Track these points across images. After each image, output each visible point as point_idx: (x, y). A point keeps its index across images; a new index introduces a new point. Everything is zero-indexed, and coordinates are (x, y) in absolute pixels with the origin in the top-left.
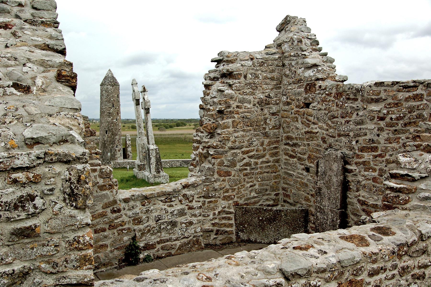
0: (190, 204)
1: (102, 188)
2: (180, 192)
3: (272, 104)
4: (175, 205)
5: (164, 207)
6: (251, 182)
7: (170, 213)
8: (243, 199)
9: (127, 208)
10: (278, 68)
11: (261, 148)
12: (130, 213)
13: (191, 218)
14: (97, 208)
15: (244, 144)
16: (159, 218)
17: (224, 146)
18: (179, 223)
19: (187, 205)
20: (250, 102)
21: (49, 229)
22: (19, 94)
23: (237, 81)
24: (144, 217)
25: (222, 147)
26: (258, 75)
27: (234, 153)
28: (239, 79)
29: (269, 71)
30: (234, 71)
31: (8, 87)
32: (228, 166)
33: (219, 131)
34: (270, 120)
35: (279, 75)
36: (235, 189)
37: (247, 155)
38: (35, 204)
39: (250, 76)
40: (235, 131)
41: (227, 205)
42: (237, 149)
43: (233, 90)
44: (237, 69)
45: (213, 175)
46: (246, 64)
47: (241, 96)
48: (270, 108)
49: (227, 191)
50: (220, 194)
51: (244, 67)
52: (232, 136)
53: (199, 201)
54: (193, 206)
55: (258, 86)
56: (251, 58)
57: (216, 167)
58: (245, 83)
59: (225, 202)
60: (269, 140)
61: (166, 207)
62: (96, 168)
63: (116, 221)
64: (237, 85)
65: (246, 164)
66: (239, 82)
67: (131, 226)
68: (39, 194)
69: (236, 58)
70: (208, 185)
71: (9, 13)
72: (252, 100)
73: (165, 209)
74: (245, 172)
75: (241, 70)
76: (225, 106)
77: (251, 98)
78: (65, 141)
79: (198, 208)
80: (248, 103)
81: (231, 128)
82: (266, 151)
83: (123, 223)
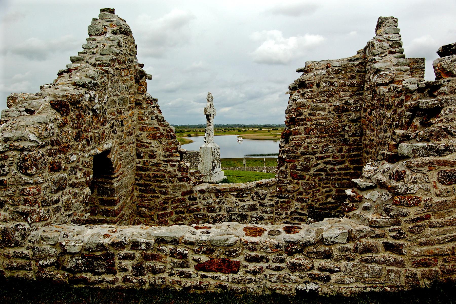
0: (261, 201)
1: (181, 179)
2: (252, 190)
3: (351, 110)
4: (247, 200)
5: (235, 201)
6: (327, 187)
7: (242, 207)
8: (319, 203)
9: (202, 198)
10: (359, 74)
11: (338, 154)
12: (205, 202)
13: (262, 214)
14: (177, 195)
15: (318, 150)
16: (230, 209)
17: (296, 151)
18: (249, 217)
19: (258, 202)
20: (324, 110)
21: (10, 182)
22: (27, 115)
23: (308, 90)
24: (217, 207)
25: (294, 152)
26: (334, 83)
27: (307, 158)
28: (311, 88)
29: (347, 78)
30: (306, 81)
31: (23, 111)
32: (300, 170)
33: (291, 137)
34: (350, 127)
35: (361, 81)
36: (309, 193)
37: (322, 160)
38: (4, 170)
39: (324, 84)
40: (308, 138)
41: (300, 207)
42: (310, 154)
43: (305, 98)
44: (309, 78)
45: (286, 177)
46: (319, 73)
47: (314, 104)
48: (349, 115)
49: (301, 194)
50: (293, 196)
51: (317, 77)
52: (304, 142)
53: (272, 200)
54: (265, 204)
55: (334, 93)
56: (327, 67)
57: (289, 170)
58: (318, 92)
59: (298, 204)
60: (348, 147)
61: (237, 201)
62: (175, 163)
63: (192, 207)
64: (308, 93)
65: (321, 170)
66: (311, 91)
67: (205, 212)
68: (7, 165)
69: (313, 67)
70: (280, 186)
71: (83, 60)
72: (327, 107)
73: (236, 203)
74: (320, 177)
75: (313, 79)
76: (295, 114)
77: (327, 105)
78: (21, 140)
79: (269, 206)
80: (322, 110)
81: (303, 134)
82: (346, 158)
83: (198, 210)
